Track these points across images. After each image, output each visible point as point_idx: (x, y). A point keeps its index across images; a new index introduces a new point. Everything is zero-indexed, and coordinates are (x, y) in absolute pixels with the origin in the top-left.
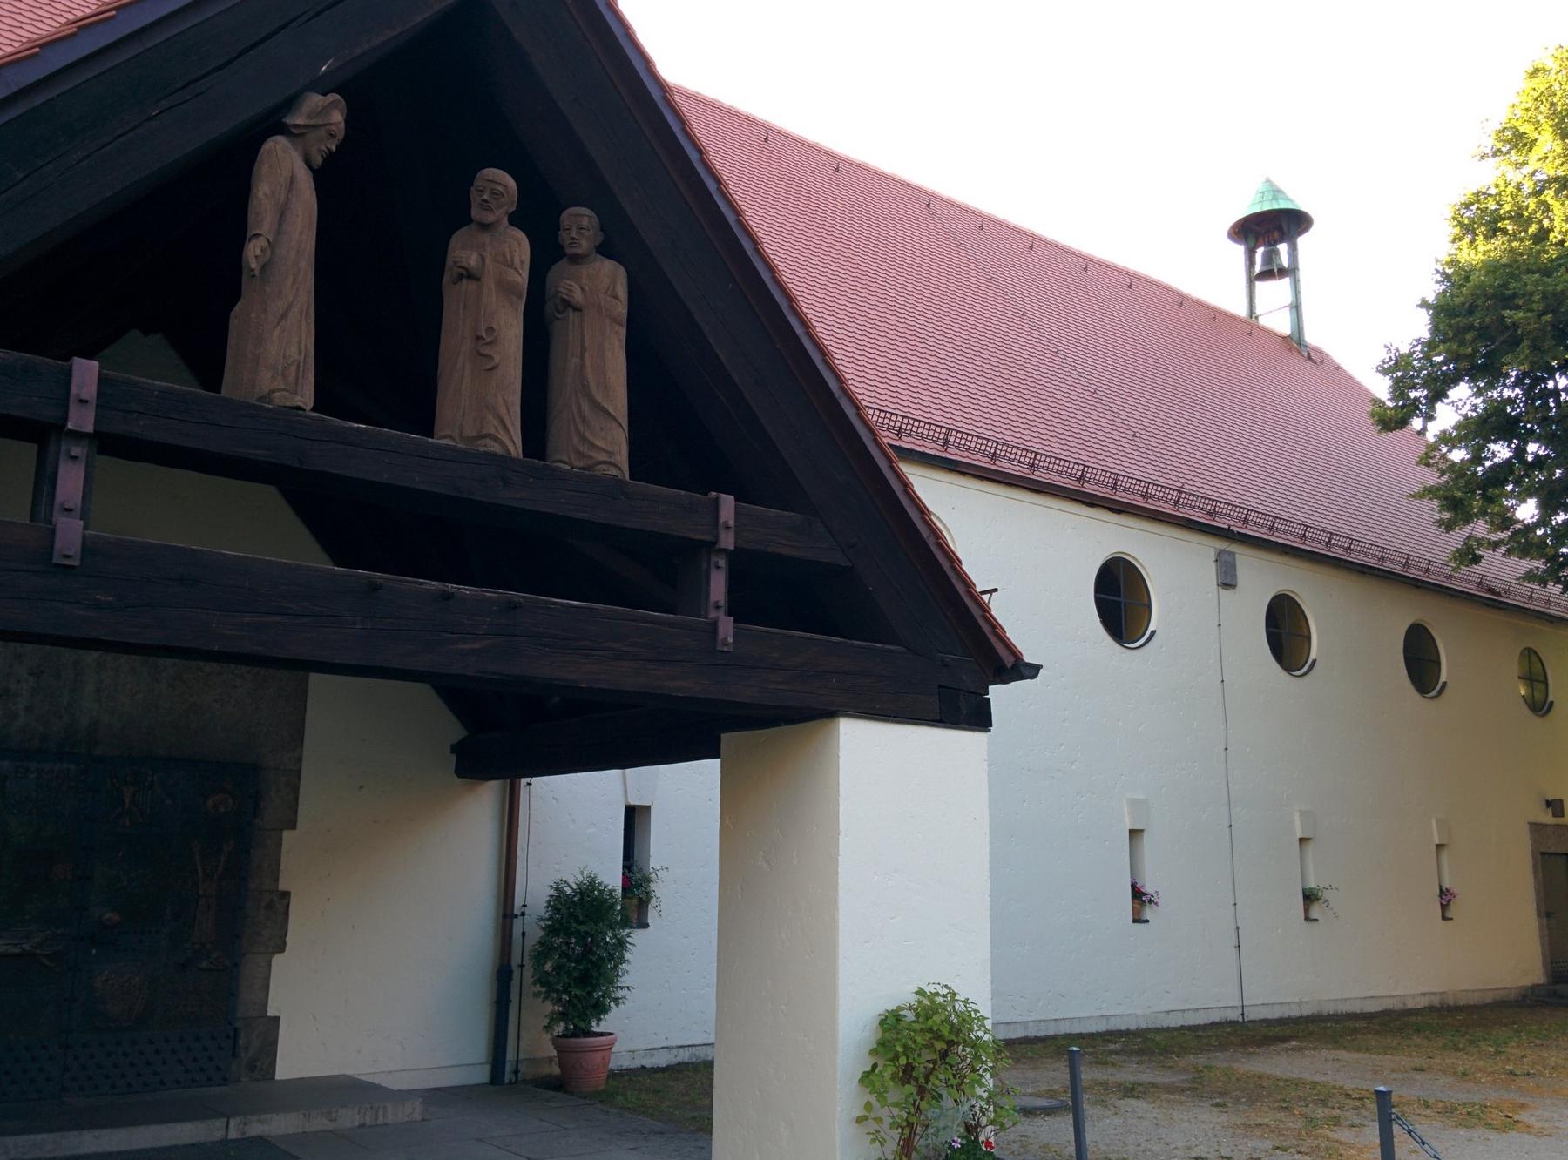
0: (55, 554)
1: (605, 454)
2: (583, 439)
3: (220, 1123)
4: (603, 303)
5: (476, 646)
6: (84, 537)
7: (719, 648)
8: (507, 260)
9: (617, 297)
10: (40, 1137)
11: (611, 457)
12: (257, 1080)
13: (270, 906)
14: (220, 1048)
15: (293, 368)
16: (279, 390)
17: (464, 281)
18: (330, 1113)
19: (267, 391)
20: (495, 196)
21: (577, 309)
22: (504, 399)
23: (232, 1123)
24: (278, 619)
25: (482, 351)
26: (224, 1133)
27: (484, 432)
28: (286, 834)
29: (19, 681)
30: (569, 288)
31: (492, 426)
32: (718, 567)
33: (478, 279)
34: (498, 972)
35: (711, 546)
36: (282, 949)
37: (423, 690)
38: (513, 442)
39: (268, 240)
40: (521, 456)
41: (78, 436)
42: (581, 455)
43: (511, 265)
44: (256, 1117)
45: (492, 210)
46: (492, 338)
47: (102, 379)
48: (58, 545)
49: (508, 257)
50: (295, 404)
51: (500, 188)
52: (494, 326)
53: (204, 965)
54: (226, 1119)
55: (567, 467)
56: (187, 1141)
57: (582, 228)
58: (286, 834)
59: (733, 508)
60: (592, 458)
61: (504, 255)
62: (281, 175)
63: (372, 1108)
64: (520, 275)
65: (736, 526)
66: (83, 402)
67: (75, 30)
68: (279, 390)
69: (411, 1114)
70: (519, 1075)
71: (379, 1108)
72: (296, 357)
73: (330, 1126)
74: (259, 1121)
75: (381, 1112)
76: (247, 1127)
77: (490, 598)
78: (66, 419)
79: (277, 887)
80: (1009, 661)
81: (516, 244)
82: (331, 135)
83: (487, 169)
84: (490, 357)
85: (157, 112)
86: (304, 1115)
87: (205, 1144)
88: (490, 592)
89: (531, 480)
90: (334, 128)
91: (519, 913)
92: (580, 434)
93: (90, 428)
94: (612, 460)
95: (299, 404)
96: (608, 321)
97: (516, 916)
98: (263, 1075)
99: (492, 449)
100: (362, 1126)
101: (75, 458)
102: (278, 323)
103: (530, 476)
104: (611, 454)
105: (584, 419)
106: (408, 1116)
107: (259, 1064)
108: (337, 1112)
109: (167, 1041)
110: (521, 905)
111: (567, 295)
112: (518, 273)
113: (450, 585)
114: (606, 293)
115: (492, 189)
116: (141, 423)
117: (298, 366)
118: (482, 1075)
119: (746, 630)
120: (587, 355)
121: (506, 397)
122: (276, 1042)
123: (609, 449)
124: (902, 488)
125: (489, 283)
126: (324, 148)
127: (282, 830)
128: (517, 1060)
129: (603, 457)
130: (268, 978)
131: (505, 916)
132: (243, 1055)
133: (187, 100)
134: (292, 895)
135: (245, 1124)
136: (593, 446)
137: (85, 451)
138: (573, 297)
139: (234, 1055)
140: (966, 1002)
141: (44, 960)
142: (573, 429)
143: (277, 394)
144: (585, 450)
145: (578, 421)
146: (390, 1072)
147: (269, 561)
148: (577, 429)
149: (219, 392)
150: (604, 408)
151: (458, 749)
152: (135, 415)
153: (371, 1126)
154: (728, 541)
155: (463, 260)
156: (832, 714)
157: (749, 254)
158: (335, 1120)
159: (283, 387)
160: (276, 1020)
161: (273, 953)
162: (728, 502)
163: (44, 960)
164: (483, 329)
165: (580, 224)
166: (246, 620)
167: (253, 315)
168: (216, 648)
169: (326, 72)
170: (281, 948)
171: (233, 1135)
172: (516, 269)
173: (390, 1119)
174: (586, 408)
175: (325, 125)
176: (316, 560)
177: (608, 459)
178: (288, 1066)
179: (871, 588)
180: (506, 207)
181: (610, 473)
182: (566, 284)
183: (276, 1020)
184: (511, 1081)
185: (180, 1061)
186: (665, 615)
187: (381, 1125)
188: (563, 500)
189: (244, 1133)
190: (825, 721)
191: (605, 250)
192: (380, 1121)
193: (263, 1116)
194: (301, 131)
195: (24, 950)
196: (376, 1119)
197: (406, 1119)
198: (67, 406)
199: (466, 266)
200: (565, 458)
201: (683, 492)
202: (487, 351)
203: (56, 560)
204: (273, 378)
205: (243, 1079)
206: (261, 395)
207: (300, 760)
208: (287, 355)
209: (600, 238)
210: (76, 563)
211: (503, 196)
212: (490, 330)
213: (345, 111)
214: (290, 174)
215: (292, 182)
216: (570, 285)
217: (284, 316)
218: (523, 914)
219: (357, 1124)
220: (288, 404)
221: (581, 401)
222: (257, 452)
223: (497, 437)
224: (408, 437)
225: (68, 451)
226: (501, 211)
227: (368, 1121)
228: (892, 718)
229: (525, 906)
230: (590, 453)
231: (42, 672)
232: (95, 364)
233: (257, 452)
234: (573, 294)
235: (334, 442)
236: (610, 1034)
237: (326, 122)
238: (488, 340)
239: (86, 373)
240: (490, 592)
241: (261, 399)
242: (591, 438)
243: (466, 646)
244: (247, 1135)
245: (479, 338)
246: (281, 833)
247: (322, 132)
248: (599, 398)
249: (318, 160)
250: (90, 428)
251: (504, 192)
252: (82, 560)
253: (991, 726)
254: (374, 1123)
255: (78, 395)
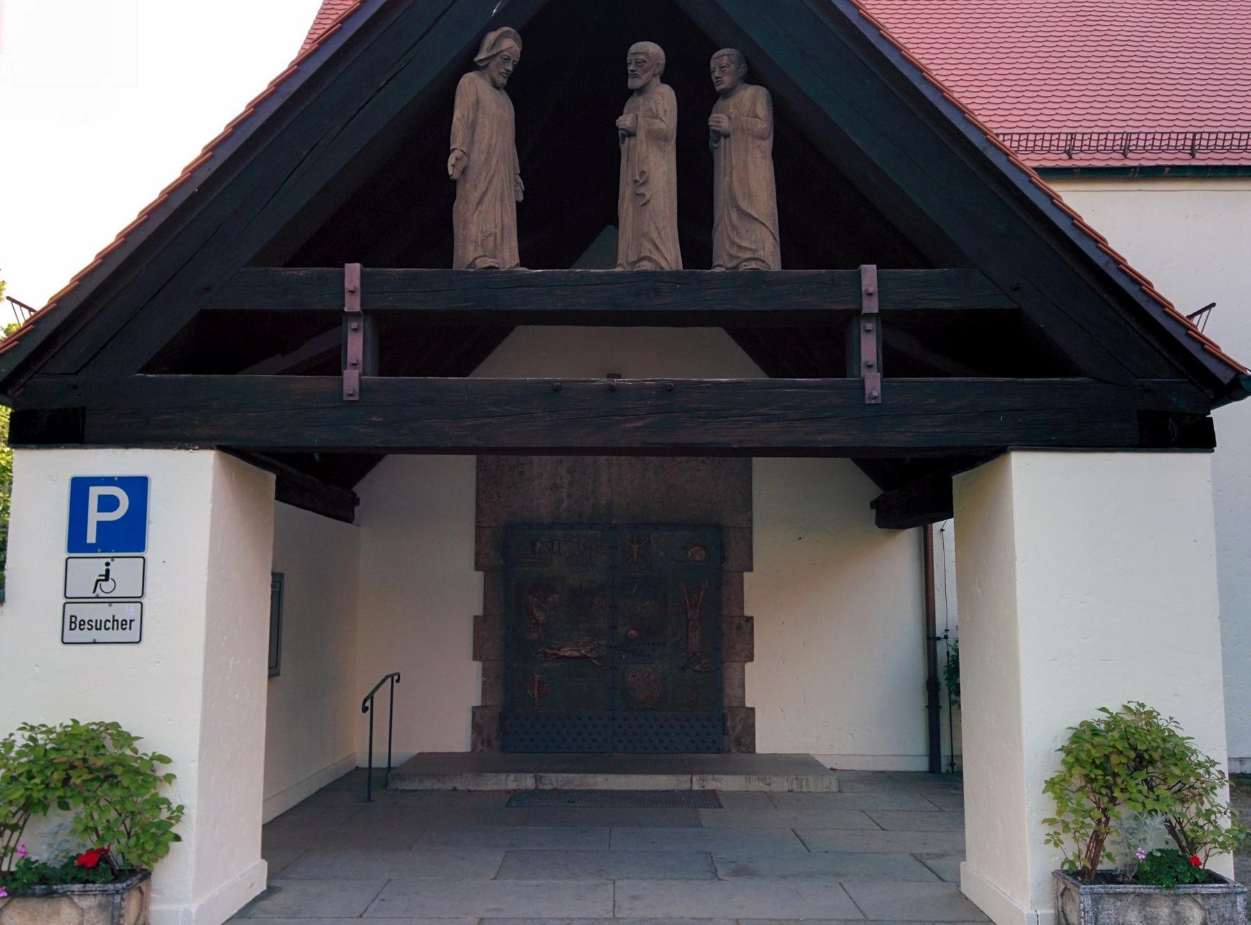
0: (344, 394)
1: (749, 252)
2: (733, 243)
3: (687, 778)
4: (744, 125)
5: (640, 424)
6: (361, 382)
7: (867, 402)
8: (654, 113)
9: (757, 117)
10: (571, 776)
11: (754, 254)
12: (743, 752)
13: (739, 627)
14: (714, 727)
15: (492, 238)
16: (480, 257)
17: (627, 139)
18: (765, 779)
19: (471, 260)
20: (640, 65)
21: (727, 136)
22: (656, 226)
23: (695, 778)
24: (490, 420)
25: (639, 192)
26: (690, 785)
27: (642, 255)
28: (746, 575)
29: (562, 478)
30: (718, 120)
31: (647, 249)
32: (868, 331)
33: (635, 135)
34: (927, 682)
35: (856, 314)
36: (751, 659)
37: (846, 464)
38: (670, 256)
39: (462, 151)
40: (681, 267)
41: (869, 316)
42: (731, 257)
43: (656, 117)
44: (711, 777)
45: (640, 77)
46: (643, 180)
47: (363, 275)
48: (345, 388)
49: (655, 111)
50: (488, 265)
51: (642, 57)
52: (645, 169)
53: (698, 668)
54: (690, 776)
55: (723, 269)
56: (663, 788)
57: (723, 67)
58: (746, 575)
59: (358, 276)
60: (739, 257)
61: (651, 109)
62: (469, 100)
63: (797, 778)
64: (664, 122)
65: (879, 291)
66: (870, 294)
67: (317, 45)
68: (480, 257)
69: (829, 786)
70: (955, 767)
71: (802, 779)
72: (493, 230)
73: (766, 788)
74: (713, 779)
75: (804, 782)
76: (705, 783)
77: (650, 385)
78: (344, 306)
79: (743, 613)
80: (1225, 377)
81: (660, 97)
82: (506, 59)
83: (631, 48)
84: (643, 195)
85: (384, 82)
86: (746, 778)
87: (673, 791)
88: (648, 381)
89: (678, 286)
90: (506, 53)
91: (942, 636)
92: (730, 238)
93: (876, 311)
94: (756, 256)
95: (491, 264)
96: (750, 139)
97: (939, 639)
98: (747, 749)
99: (644, 268)
100: (790, 791)
101: (868, 331)
102: (476, 209)
103: (677, 284)
104: (754, 251)
105: (734, 227)
106: (826, 788)
107: (742, 740)
108: (770, 779)
109: (590, 719)
110: (944, 630)
111: (716, 126)
112: (662, 120)
113: (615, 380)
114: (748, 116)
115: (637, 60)
116: (390, 299)
117: (496, 236)
118: (922, 765)
119: (896, 382)
120: (734, 172)
121: (657, 225)
122: (753, 726)
123: (753, 247)
124: (1069, 221)
125: (641, 135)
126: (503, 70)
127: (743, 572)
128: (952, 756)
129: (748, 255)
130: (743, 679)
131: (928, 638)
132: (731, 733)
133: (403, 68)
134: (755, 619)
135: (704, 781)
136: (740, 247)
137: (362, 324)
138: (721, 127)
139: (725, 733)
140: (61, 725)
141: (595, 661)
142: (726, 237)
143: (478, 260)
144: (734, 252)
145: (729, 229)
146: (844, 755)
147: (480, 380)
148: (729, 236)
149: (452, 268)
150: (748, 213)
151: (875, 504)
152: (386, 295)
153: (797, 792)
154: (871, 306)
155: (723, 121)
156: (997, 451)
157: (873, 41)
158: (770, 784)
159: (482, 254)
160: (753, 710)
161: (746, 662)
162: (869, 274)
163: (595, 661)
164: (637, 174)
165: (724, 64)
166: (468, 423)
167: (461, 207)
168: (449, 445)
169: (497, 13)
170: (751, 658)
171: (696, 787)
172: (660, 118)
173: (812, 789)
174: (734, 216)
175: (499, 53)
176: (762, 378)
177: (753, 256)
178: (765, 743)
179: (1042, 326)
180: (652, 70)
181: (750, 267)
182: (715, 117)
183: (753, 710)
184: (948, 771)
185: (687, 735)
186: (812, 380)
187: (805, 792)
188: (708, 298)
189: (703, 787)
190: (996, 461)
191: (752, 78)
192: (805, 789)
193: (716, 776)
194: (486, 63)
195: (581, 654)
196: (801, 787)
197: (826, 790)
198: (344, 297)
199: (624, 127)
200: (721, 263)
201: (823, 271)
202: (642, 190)
203: (345, 398)
204: (475, 250)
205: (733, 750)
206: (469, 263)
207: (751, 520)
208: (484, 230)
209: (743, 69)
210: (356, 398)
211: (645, 62)
212: (643, 173)
213: (521, 41)
214: (476, 98)
215: (478, 104)
216: (719, 117)
217: (480, 202)
218: (946, 637)
219: (787, 789)
220: (484, 266)
221: (731, 212)
222: (466, 304)
223: (651, 258)
224: (575, 272)
225: (865, 327)
226: (647, 75)
227: (795, 788)
228: (1075, 448)
229: (947, 630)
230: (738, 255)
231: (575, 471)
232: (358, 265)
233: (466, 304)
234: (721, 124)
235: (520, 287)
236: (1193, 738)
237: (499, 50)
238: (641, 182)
239: (353, 271)
240: (648, 381)
241: (469, 266)
242: (738, 241)
243: (632, 425)
244: (706, 788)
245: (636, 181)
246: (743, 574)
247: (498, 59)
248: (744, 205)
249: (502, 81)
250: (876, 311)
251: (645, 59)
252: (360, 395)
253: (1215, 446)
254: (799, 790)
255: (866, 290)
